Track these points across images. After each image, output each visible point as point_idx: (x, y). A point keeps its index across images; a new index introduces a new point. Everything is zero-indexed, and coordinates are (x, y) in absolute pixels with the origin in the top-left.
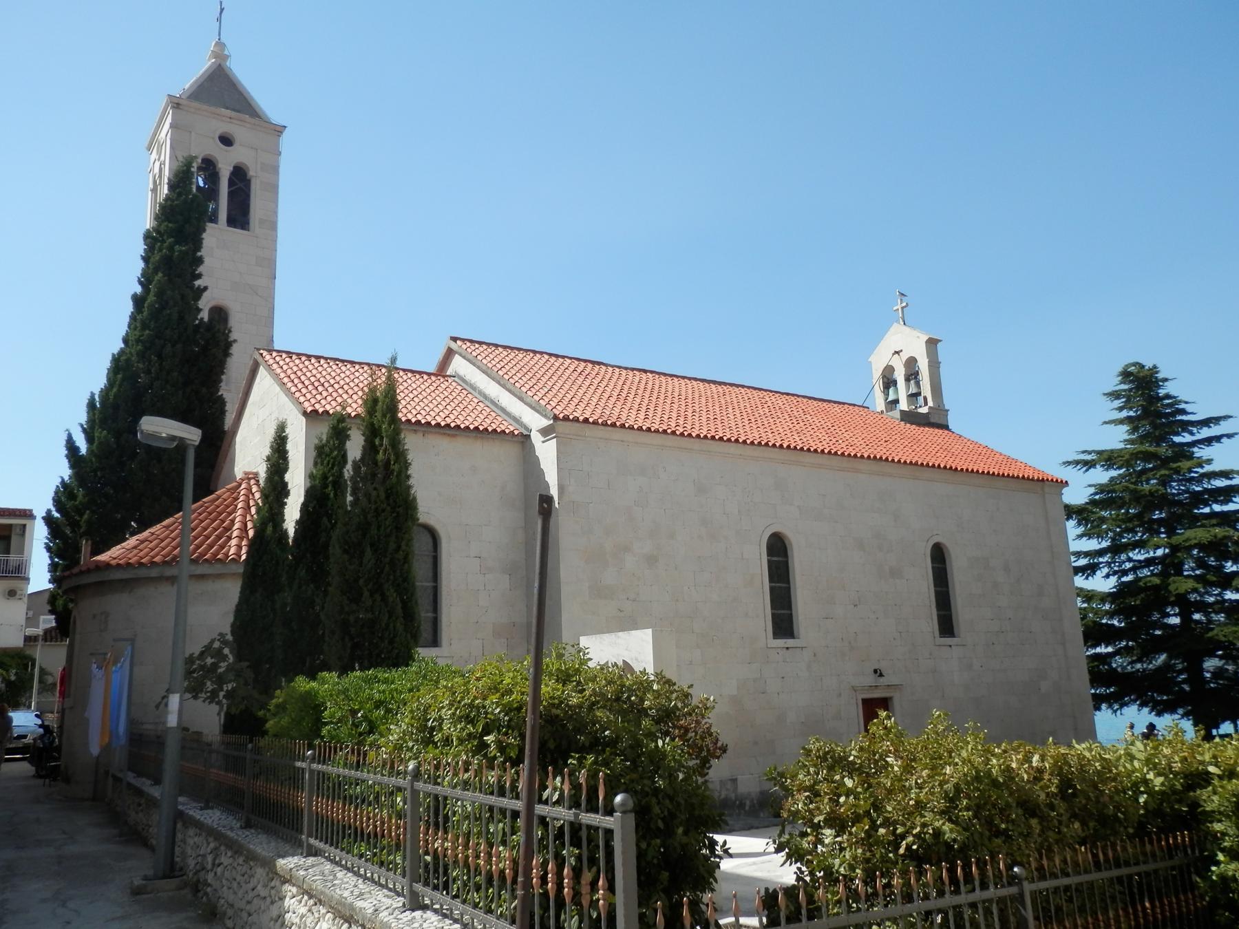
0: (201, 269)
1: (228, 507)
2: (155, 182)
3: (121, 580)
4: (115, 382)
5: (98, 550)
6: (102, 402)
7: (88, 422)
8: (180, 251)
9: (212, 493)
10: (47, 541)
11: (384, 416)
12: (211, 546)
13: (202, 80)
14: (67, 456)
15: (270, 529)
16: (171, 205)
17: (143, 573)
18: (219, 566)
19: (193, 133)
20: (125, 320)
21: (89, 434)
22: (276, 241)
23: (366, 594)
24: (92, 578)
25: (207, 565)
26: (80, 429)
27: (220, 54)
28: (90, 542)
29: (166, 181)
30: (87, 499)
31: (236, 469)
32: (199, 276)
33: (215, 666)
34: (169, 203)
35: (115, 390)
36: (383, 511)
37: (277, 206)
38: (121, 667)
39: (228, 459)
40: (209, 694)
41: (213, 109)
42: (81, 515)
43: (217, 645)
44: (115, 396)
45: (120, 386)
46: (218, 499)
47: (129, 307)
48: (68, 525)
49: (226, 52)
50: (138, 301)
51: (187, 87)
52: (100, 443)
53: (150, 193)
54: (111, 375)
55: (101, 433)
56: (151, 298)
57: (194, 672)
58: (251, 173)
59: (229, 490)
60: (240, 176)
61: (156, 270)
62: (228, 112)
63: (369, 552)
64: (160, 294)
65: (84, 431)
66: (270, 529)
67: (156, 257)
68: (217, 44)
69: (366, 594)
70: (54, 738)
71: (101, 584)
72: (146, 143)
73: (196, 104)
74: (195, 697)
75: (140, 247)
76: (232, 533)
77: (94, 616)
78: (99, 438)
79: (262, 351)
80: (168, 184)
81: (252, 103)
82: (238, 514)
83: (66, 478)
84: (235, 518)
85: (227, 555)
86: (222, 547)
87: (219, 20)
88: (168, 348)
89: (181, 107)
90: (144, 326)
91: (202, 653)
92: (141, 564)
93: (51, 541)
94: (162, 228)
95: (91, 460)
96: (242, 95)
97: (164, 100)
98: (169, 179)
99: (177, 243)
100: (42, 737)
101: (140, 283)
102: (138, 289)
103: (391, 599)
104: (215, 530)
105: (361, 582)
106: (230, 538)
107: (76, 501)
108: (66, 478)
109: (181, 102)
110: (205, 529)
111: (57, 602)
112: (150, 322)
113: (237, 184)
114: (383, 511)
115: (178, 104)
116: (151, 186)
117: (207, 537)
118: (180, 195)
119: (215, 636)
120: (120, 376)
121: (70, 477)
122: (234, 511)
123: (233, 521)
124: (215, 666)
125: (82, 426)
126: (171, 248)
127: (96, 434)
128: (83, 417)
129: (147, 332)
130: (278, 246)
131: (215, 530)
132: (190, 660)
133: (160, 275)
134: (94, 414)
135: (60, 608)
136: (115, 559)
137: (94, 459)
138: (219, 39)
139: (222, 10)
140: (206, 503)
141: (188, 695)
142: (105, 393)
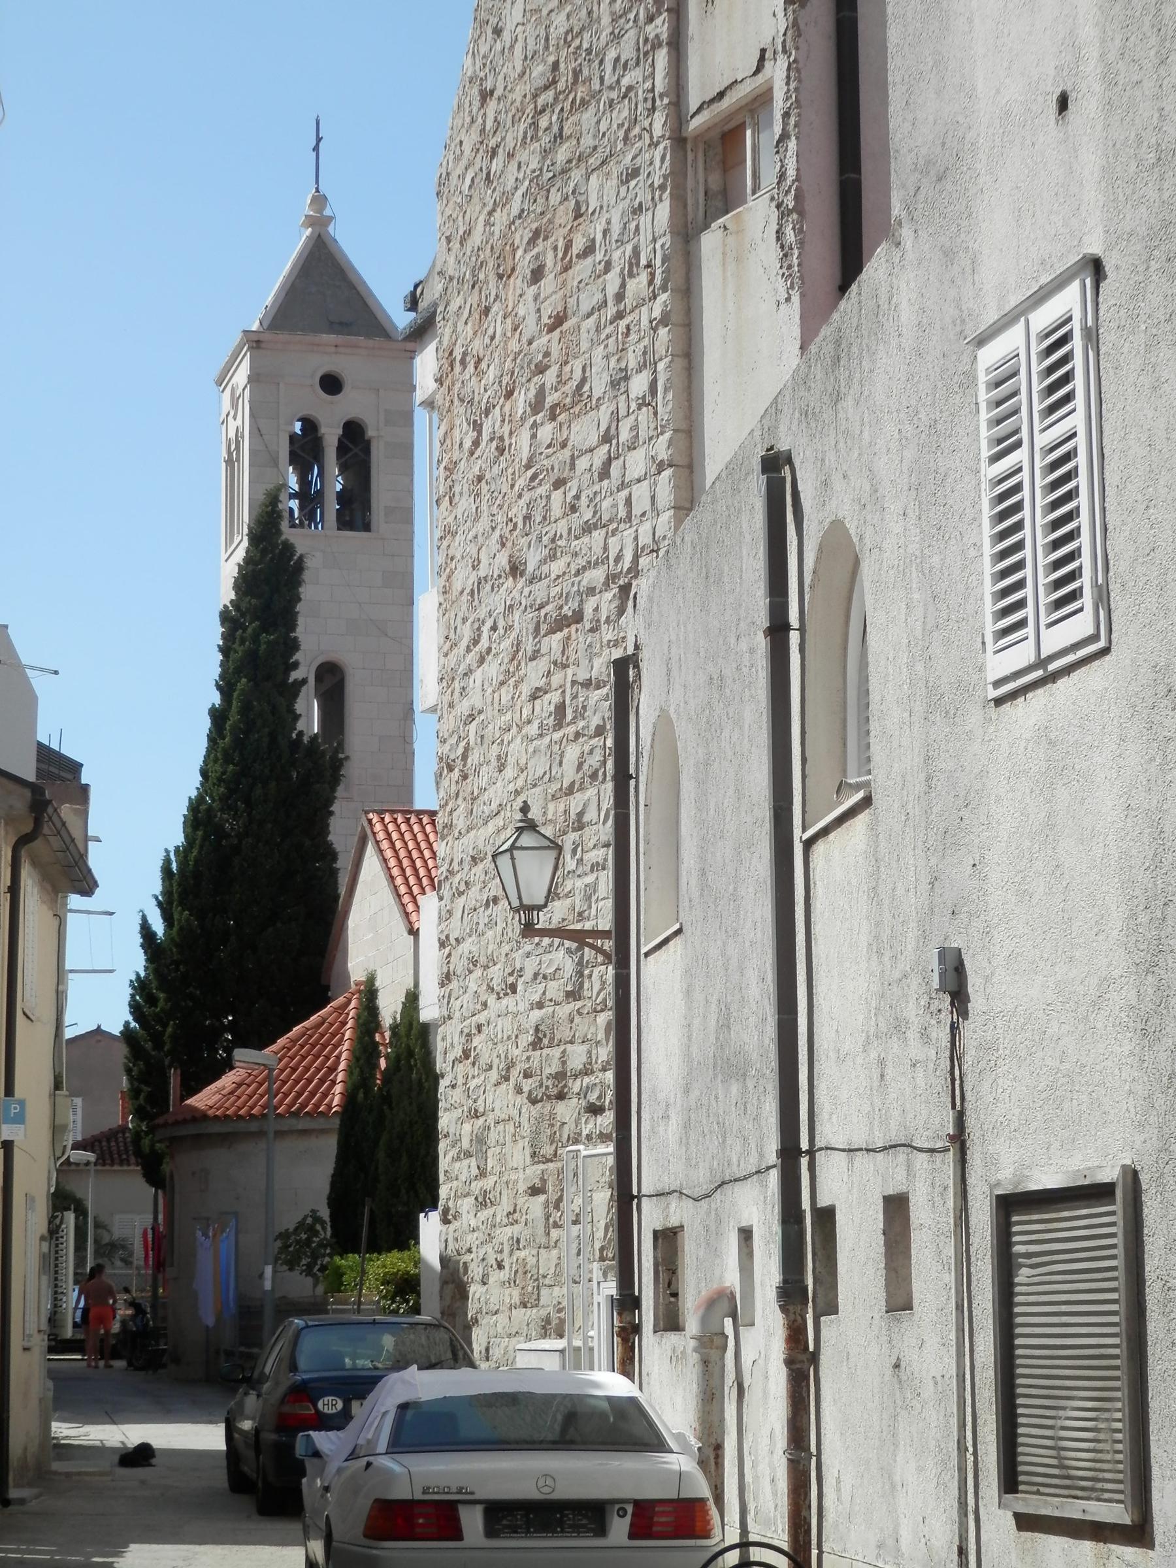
0: (298, 656)
1: (334, 1035)
2: (230, 453)
3: (219, 1134)
4: (195, 840)
5: (192, 1086)
6: (182, 864)
7: (163, 893)
8: (268, 643)
9: (326, 1001)
10: (126, 1061)
11: (417, 1040)
12: (313, 1094)
13: (293, 278)
14: (142, 946)
15: (361, 1095)
16: (253, 571)
17: (241, 1126)
18: (322, 1120)
19: (281, 385)
20: (202, 745)
21: (166, 908)
22: (412, 540)
23: (403, 1191)
24: (191, 1130)
25: (308, 1118)
26: (155, 903)
27: (319, 222)
28: (179, 1071)
29: (246, 531)
30: (169, 1004)
31: (349, 965)
32: (296, 665)
33: (308, 1242)
34: (250, 567)
35: (195, 852)
36: (416, 1122)
37: (412, 480)
38: (227, 1237)
39: (341, 945)
40: (304, 1268)
41: (310, 338)
42: (165, 1026)
43: (309, 1221)
44: (196, 861)
45: (201, 847)
46: (323, 1023)
47: (206, 724)
48: (149, 1040)
49: (327, 212)
50: (218, 716)
51: (269, 300)
52: (181, 929)
53: (224, 464)
54: (189, 830)
55: (181, 913)
56: (234, 717)
57: (290, 1246)
58: (370, 433)
59: (336, 1009)
60: (354, 434)
61: (238, 671)
62: (332, 338)
63: (405, 1159)
64: (245, 709)
65: (160, 904)
66: (361, 1095)
67: (239, 651)
68: (314, 199)
69: (403, 1191)
70: (148, 1321)
71: (198, 1137)
72: (215, 373)
73: (283, 337)
74: (291, 1269)
75: (215, 633)
76: (336, 1076)
77: (194, 1173)
78: (179, 921)
79: (371, 816)
80: (247, 535)
81: (370, 302)
82: (345, 1047)
83: (143, 974)
84: (341, 1053)
85: (329, 1107)
86: (325, 1095)
87: (316, 149)
88: (258, 791)
89: (263, 345)
90: (227, 759)
91: (296, 1229)
92: (240, 1117)
93: (130, 1061)
94: (244, 606)
95: (171, 950)
96: (355, 288)
97: (237, 337)
98: (249, 527)
99: (264, 629)
100: (133, 1318)
101: (218, 687)
102: (216, 698)
103: (421, 1196)
104: (318, 1070)
105: (399, 1181)
106: (334, 1083)
107: (157, 1007)
108: (143, 974)
109: (262, 337)
110: (307, 1069)
111: (143, 1141)
112: (234, 752)
113: (351, 450)
114: (416, 1122)
115: (258, 342)
116: (225, 455)
117: (310, 1081)
118: (264, 552)
119: (308, 1212)
120: (200, 833)
121: (146, 968)
122: (340, 1043)
123: (338, 1057)
124: (308, 1242)
125: (156, 898)
126: (255, 638)
127: (176, 916)
128: (157, 887)
129: (231, 767)
130: (416, 548)
131: (318, 1070)
132: (284, 1236)
133: (244, 680)
134: (171, 885)
135: (146, 1150)
136: (211, 1107)
137: (174, 950)
138: (317, 190)
139: (319, 140)
140: (308, 1029)
141: (285, 1267)
142: (183, 853)
